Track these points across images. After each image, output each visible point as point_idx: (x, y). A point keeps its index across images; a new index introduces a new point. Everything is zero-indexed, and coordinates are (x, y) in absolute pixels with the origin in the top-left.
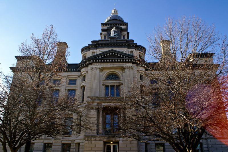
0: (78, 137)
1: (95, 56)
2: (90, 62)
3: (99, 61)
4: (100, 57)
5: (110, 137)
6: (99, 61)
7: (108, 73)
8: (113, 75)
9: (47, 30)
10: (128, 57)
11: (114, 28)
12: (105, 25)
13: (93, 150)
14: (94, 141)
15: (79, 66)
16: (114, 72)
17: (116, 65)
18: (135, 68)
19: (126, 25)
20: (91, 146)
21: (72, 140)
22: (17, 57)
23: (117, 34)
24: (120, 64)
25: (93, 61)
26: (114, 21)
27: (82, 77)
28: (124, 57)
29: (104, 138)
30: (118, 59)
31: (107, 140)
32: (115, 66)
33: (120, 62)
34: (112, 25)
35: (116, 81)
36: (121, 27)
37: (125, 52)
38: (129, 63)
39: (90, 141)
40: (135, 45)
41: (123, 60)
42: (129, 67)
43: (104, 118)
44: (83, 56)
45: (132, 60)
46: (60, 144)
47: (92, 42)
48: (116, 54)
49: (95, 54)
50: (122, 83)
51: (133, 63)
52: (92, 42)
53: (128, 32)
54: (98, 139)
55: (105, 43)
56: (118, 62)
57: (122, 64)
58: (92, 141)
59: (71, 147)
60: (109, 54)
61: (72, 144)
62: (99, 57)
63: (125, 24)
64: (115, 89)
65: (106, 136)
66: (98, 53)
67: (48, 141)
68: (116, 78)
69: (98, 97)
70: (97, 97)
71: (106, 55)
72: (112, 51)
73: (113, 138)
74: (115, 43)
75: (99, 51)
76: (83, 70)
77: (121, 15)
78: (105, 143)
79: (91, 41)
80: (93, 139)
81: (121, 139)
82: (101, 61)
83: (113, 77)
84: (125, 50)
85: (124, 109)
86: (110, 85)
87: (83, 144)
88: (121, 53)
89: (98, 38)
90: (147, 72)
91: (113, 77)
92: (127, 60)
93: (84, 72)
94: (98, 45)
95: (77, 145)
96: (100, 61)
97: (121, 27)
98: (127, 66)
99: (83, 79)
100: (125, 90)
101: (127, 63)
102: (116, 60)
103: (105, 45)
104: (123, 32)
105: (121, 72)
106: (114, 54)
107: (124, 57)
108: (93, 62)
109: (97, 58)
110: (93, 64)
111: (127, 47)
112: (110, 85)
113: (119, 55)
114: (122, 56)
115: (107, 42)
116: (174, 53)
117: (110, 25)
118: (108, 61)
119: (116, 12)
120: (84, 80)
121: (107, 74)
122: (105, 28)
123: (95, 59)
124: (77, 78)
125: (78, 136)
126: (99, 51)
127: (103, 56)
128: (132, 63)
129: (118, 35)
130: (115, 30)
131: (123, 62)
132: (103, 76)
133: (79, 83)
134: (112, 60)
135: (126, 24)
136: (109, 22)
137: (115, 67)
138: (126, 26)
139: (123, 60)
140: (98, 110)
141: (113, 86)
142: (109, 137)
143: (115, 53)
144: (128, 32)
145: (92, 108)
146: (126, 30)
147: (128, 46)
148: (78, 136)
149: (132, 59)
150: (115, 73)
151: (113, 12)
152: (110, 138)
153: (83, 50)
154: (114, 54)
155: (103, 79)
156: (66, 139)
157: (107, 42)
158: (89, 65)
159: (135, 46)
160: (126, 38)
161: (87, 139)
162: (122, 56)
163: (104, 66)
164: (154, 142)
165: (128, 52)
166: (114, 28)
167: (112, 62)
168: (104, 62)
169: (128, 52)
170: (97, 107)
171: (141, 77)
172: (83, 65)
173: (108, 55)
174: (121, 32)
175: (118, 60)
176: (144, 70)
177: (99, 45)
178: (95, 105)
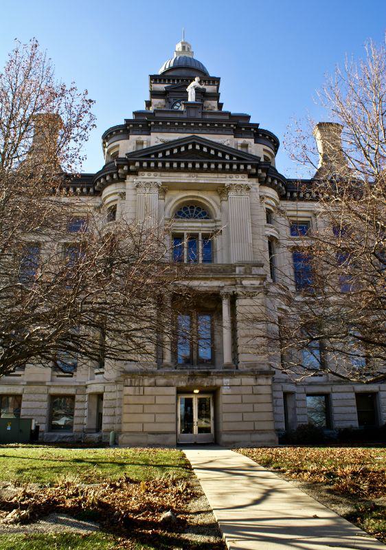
0: (96, 376)
2: (132, 168)
3: (231, 165)
4: (160, 155)
5: (195, 375)
6: (231, 165)
10: (238, 158)
11: (197, 79)
12: (160, 80)
13: (245, 403)
15: (99, 180)
16: (197, 197)
17: (204, 178)
18: (256, 189)
20: (143, 400)
21: (78, 384)
24: (216, 175)
27: (105, 210)
29: (180, 377)
31: (189, 384)
32: (201, 181)
33: (216, 171)
34: (178, 81)
35: (202, 222)
38: (240, 176)
39: (137, 388)
41: (224, 166)
42: (240, 186)
45: (249, 167)
46: (45, 397)
51: (251, 176)
53: (220, 102)
54: (162, 381)
55: (180, 119)
57: (220, 175)
58: (144, 386)
59: (77, 405)
60: (186, 147)
61: (77, 397)
62: (156, 155)
63: (214, 82)
64: (200, 243)
65: (186, 372)
66: (153, 144)
67: (12, 387)
73: (204, 379)
74: (199, 119)
75: (154, 139)
78: (180, 391)
80: (147, 382)
81: (226, 381)
82: (164, 164)
83: (192, 212)
84: (227, 140)
85: (233, 298)
86: (185, 232)
87: (113, 396)
90: (283, 203)
91: (192, 212)
92: (235, 167)
93: (111, 195)
95: (95, 400)
96: (160, 165)
98: (233, 183)
100: (230, 250)
101: (234, 175)
102: (205, 166)
103: (180, 123)
105: (217, 199)
106: (198, 147)
108: (141, 168)
109: (153, 156)
110: (140, 173)
113: (212, 152)
115: (178, 115)
117: (174, 81)
118: (183, 165)
119: (186, 50)
120: (114, 218)
121: (177, 204)
122: (161, 87)
123: (145, 160)
125: (97, 374)
126: (154, 139)
127: (168, 153)
128: (246, 175)
130: (198, 85)
131: (224, 171)
132: (167, 210)
135: (216, 81)
136: (170, 73)
137: (202, 183)
138: (216, 87)
139: (224, 166)
141: (193, 237)
143: (202, 147)
144: (220, 102)
147: (234, 130)
148: (97, 374)
149: (249, 164)
150: (199, 200)
151: (180, 50)
154: (198, 147)
155: (167, 217)
156: (62, 384)
157: (178, 115)
158: (128, 176)
159: (252, 130)
161: (131, 381)
163: (172, 181)
164: (303, 391)
166: (196, 79)
167: (194, 170)
168: (171, 170)
172: (111, 175)
173: (183, 149)
175: (209, 165)
177: (157, 123)
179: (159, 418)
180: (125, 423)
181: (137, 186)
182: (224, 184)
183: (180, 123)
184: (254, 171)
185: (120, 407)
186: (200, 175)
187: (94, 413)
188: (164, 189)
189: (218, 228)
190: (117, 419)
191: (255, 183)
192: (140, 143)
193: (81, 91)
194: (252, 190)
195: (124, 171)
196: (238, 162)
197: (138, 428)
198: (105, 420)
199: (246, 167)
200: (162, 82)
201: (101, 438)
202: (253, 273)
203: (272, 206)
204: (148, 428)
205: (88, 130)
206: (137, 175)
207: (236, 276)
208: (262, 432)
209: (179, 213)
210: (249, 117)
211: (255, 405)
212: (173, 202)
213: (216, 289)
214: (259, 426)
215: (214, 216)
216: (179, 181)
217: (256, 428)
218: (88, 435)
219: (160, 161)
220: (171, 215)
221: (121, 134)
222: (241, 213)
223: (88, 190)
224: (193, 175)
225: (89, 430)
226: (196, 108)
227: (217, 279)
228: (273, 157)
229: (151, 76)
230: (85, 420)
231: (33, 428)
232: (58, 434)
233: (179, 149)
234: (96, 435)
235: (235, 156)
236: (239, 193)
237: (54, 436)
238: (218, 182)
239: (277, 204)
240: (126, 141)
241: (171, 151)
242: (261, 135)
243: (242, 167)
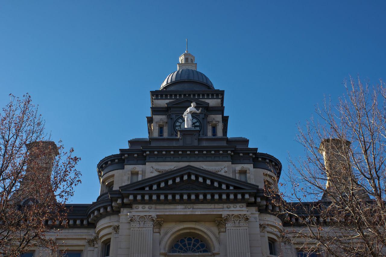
1: (139, 183)
2: (125, 201)
3: (228, 196)
4: (155, 187)
6: (228, 196)
7: (176, 232)
8: (189, 239)
9: (13, 108)
10: (235, 188)
12: (162, 96)
15: (93, 212)
16: (195, 229)
17: (200, 210)
18: (255, 218)
19: (220, 97)
24: (212, 206)
25: (135, 197)
26: (186, 87)
27: (99, 245)
28: (224, 187)
30: (207, 191)
32: (197, 213)
33: (213, 201)
34: (180, 95)
36: (207, 101)
37: (224, 174)
40: (253, 154)
41: (220, 196)
42: (238, 216)
44: (103, 182)
45: (247, 196)
47: (131, 142)
48: (201, 180)
49: (140, 178)
51: (249, 205)
52: (131, 142)
53: (225, 115)
56: (205, 201)
57: (217, 206)
60: (182, 177)
62: (151, 187)
63: (217, 95)
66: (148, 175)
68: (198, 248)
71: (170, 182)
72: (189, 171)
75: (150, 170)
76: (102, 223)
77: (202, 68)
79: (129, 142)
82: (158, 197)
83: (189, 244)
84: (224, 168)
88: (214, 176)
89: (142, 133)
91: (189, 244)
92: (232, 197)
94: (148, 153)
96: (154, 197)
97: (207, 101)
98: (231, 213)
101: (232, 205)
103: (168, 152)
104: (213, 116)
105: (215, 229)
106: (193, 177)
107: (224, 187)
108: (135, 201)
110: (134, 206)
111: (230, 159)
113: (208, 182)
114: (216, 184)
115: (174, 144)
116: (375, 175)
117: (176, 95)
118: (178, 197)
119: (190, 61)
124: (84, 246)
126: (150, 170)
128: (244, 205)
129: (198, 124)
130: (194, 110)
131: (220, 201)
132: (163, 243)
134: (181, 196)
135: (220, 94)
139: (220, 196)
144: (225, 115)
146: (220, 110)
149: (247, 193)
153: (104, 165)
154: (193, 177)
157: (174, 144)
158: (122, 209)
159: (251, 155)
160: (220, 134)
162: (216, 184)
163: (167, 213)
165: (234, 172)
167: (189, 201)
168: (166, 202)
169: (234, 172)
172: (105, 208)
173: (178, 180)
174: (206, 116)
176: (279, 223)
181: (131, 220)
182: (221, 215)
183: (176, 152)
184: (253, 200)
186: (196, 206)
188: (159, 222)
191: (254, 212)
192: (134, 174)
193: (67, 149)
194: (252, 219)
195: (118, 204)
196: (235, 191)
199: (243, 196)
200: (164, 97)
203: (276, 235)
205: (73, 185)
206: (131, 208)
209: (176, 246)
210: (246, 141)
215: (212, 248)
216: (175, 213)
219: (155, 194)
220: (167, 249)
221: (117, 163)
223: (82, 222)
224: (189, 206)
226: (192, 134)
228: (276, 182)
229: (152, 92)
233: (174, 180)
235: (232, 186)
236: (237, 224)
238: (215, 213)
239: (281, 231)
241: (166, 182)
242: (260, 159)
243: (239, 196)
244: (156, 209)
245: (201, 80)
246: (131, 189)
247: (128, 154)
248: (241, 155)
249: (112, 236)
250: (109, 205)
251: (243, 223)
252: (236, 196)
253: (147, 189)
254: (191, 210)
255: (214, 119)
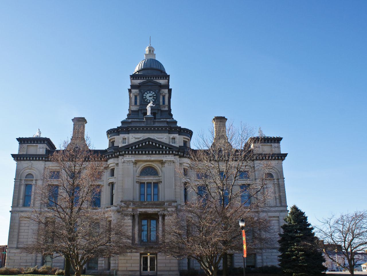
3: (166, 152)
4: (134, 148)
6: (166, 152)
10: (169, 148)
13: (128, 263)
14: (129, 253)
16: (151, 165)
17: (154, 158)
22: (19, 140)
23: (153, 93)
24: (159, 156)
25: (125, 152)
26: (149, 71)
27: (109, 170)
28: (164, 147)
31: (145, 252)
33: (159, 154)
35: (153, 177)
38: (170, 156)
41: (162, 152)
42: (170, 161)
43: (140, 226)
44: (110, 140)
45: (174, 152)
50: (161, 180)
51: (175, 155)
57: (161, 156)
60: (146, 143)
62: (132, 148)
63: (166, 78)
69: (133, 202)
70: (131, 202)
71: (140, 145)
72: (149, 139)
78: (141, 254)
85: (164, 216)
98: (167, 159)
99: (111, 171)
101: (167, 156)
107: (164, 147)
108: (125, 154)
112: (146, 182)
114: (161, 146)
119: (151, 51)
121: (142, 168)
122: (137, 82)
123: (129, 149)
127: (137, 146)
128: (173, 155)
129: (155, 95)
130: (152, 105)
132: (138, 172)
133: (106, 178)
139: (162, 152)
140: (133, 216)
141: (149, 184)
142: (146, 249)
145: (126, 215)
146: (167, 86)
152: (147, 250)
154: (151, 143)
155: (137, 175)
162: (161, 146)
170: (132, 214)
171: (185, 172)
172: (112, 155)
173: (144, 144)
174: (160, 90)
178: (129, 211)
179: (133, 265)
180: (120, 267)
182: (163, 160)
184: (177, 153)
185: (118, 260)
186: (152, 156)
187: (107, 262)
189: (160, 180)
190: (117, 265)
197: (125, 269)
198: (112, 265)
199: (173, 152)
201: (110, 272)
202: (172, 205)
204: (129, 269)
207: (165, 207)
208: (173, 271)
211: (171, 260)
212: (140, 167)
213: (157, 212)
214: (172, 269)
215: (159, 174)
217: (171, 269)
218: (105, 271)
222: (171, 171)
224: (149, 156)
225: (105, 269)
227: (157, 208)
230: (103, 265)
231: (84, 269)
232: (92, 271)
234: (108, 272)
237: (90, 272)
238: (160, 159)
240: (118, 136)
242: (182, 131)
243: (171, 152)
244: (134, 157)
245: (158, 68)
246: (123, 149)
247: (121, 129)
248: (173, 130)
249: (116, 168)
250: (114, 154)
251: (172, 164)
252: (169, 152)
253: (130, 148)
254: (150, 158)
255: (164, 92)
